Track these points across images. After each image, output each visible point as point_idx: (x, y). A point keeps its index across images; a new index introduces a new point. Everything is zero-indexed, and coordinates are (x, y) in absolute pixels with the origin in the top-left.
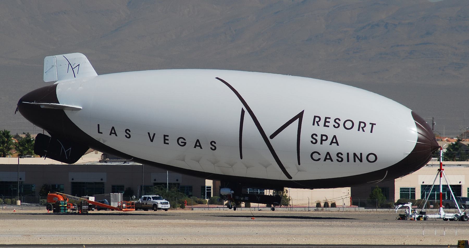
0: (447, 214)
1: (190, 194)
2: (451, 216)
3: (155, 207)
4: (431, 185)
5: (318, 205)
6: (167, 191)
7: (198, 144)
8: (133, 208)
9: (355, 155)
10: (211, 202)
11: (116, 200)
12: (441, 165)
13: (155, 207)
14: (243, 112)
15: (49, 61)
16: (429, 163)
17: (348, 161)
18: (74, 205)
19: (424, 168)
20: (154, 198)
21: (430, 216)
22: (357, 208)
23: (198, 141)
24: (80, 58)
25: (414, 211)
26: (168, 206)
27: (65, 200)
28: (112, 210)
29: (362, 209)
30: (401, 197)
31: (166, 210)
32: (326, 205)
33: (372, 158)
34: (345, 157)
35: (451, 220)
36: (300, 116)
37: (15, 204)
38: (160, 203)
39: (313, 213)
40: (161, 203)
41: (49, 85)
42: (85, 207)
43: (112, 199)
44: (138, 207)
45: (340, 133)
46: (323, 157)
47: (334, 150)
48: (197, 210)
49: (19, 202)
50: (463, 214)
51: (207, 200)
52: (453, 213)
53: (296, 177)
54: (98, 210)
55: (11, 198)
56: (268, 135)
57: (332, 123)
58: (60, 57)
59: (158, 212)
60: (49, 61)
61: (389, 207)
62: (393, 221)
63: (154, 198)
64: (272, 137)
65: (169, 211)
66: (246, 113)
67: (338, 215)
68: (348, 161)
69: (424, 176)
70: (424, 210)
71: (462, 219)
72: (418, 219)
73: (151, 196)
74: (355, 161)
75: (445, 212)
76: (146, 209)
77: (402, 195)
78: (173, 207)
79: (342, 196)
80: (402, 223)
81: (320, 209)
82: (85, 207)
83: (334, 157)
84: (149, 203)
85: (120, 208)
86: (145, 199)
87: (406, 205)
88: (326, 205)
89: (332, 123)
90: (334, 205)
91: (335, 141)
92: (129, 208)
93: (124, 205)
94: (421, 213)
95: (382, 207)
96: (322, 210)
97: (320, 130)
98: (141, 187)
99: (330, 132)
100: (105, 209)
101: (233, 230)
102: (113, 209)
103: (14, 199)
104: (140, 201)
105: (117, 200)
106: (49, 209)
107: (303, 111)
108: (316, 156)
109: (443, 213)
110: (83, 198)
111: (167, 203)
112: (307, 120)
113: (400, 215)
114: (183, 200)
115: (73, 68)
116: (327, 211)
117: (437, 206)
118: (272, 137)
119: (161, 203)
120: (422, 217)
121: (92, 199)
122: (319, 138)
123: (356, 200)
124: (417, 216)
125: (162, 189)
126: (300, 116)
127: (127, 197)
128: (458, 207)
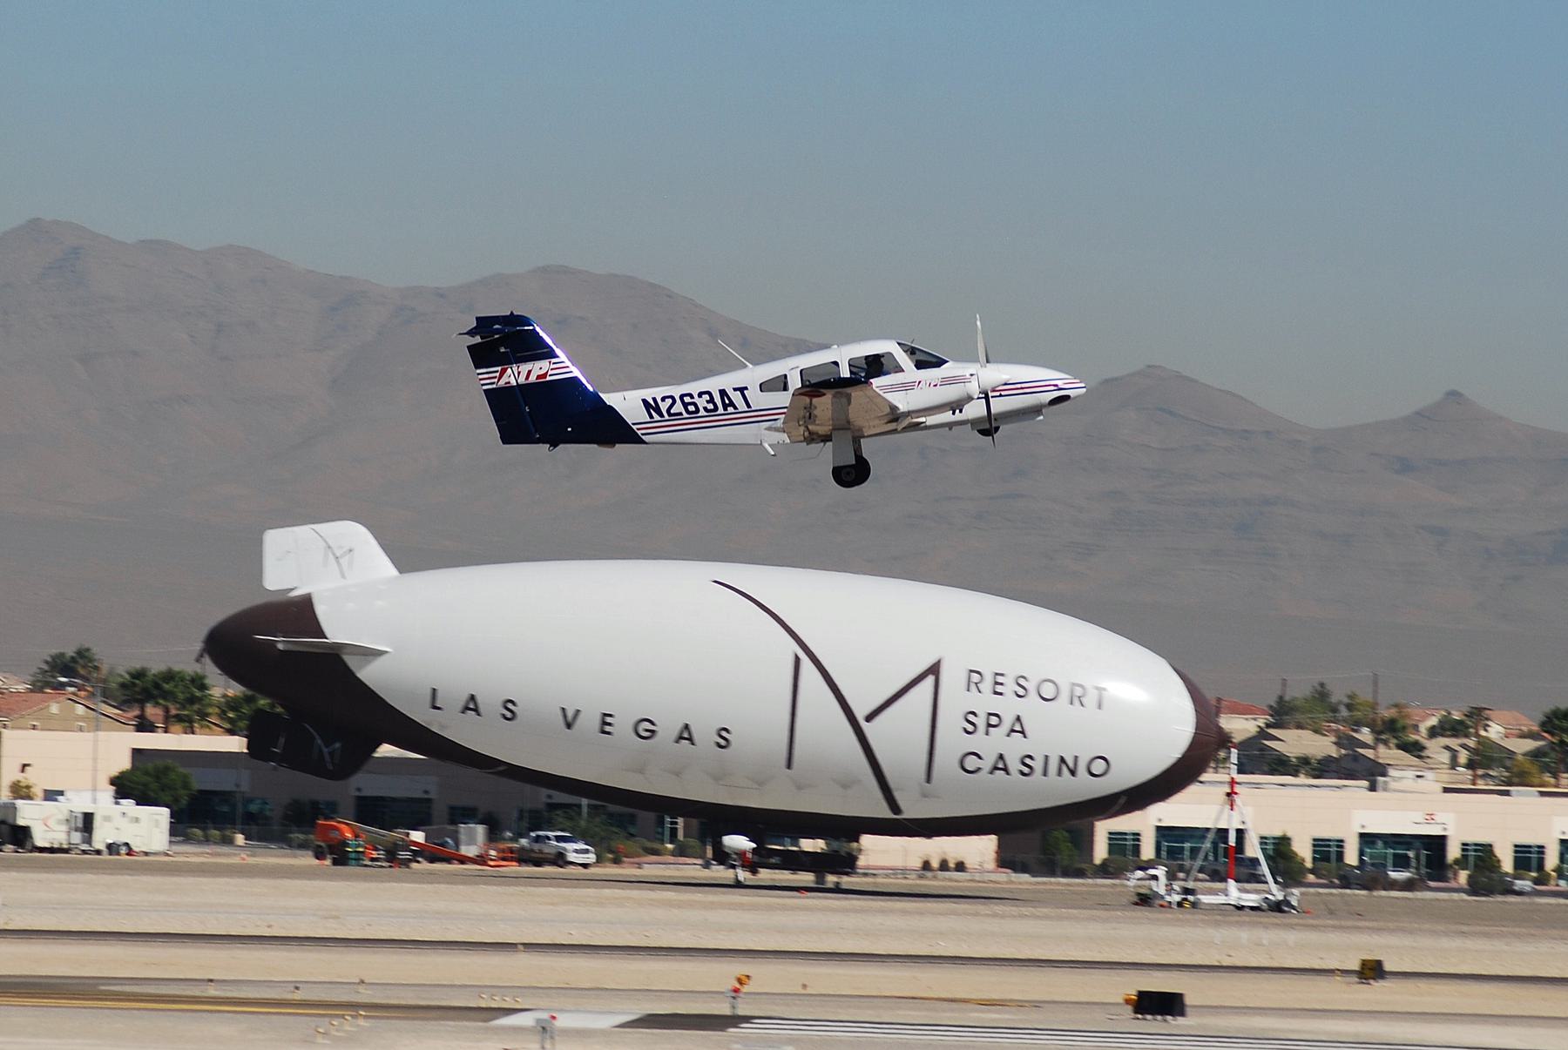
0: (1245, 896)
1: (632, 830)
2: (1251, 899)
3: (560, 860)
4: (1208, 829)
5: (926, 866)
6: (583, 823)
7: (686, 735)
8: (512, 860)
9: (1062, 760)
10: (681, 852)
11: (472, 842)
12: (1233, 783)
13: (560, 860)
14: (797, 660)
15: (277, 541)
16: (1204, 777)
17: (1045, 774)
18: (376, 849)
19: (1193, 789)
20: (558, 839)
21: (1206, 899)
22: (1015, 877)
23: (687, 727)
24: (354, 535)
25: (1170, 890)
26: (591, 858)
27: (356, 836)
28: (462, 862)
29: (1026, 877)
30: (1110, 852)
31: (585, 866)
32: (944, 866)
33: (1099, 767)
34: (1037, 765)
35: (1252, 908)
36: (934, 670)
37: (228, 841)
38: (575, 851)
39: (912, 883)
40: (576, 851)
41: (280, 598)
42: (404, 855)
43: (463, 837)
44: (524, 858)
45: (1030, 708)
46: (987, 764)
47: (1014, 749)
48: (652, 869)
49: (240, 839)
50: (1280, 897)
51: (670, 846)
52: (1257, 892)
53: (911, 811)
54: (432, 861)
55: (204, 829)
56: (860, 716)
57: (1009, 687)
58: (304, 532)
59: (570, 870)
60: (277, 541)
61: (1080, 874)
62: (1123, 907)
63: (558, 839)
64: (869, 718)
65: (592, 870)
66: (806, 661)
67: (968, 888)
68: (1045, 774)
69: (1192, 808)
70: (1190, 885)
71: (1278, 907)
72: (1180, 904)
73: (550, 834)
74: (1060, 773)
75: (1240, 890)
76: (538, 864)
77: (1112, 848)
78: (600, 860)
79: (980, 850)
80: (1143, 912)
81: (929, 874)
82: (404, 855)
83: (1014, 765)
84: (546, 850)
85: (481, 860)
86: (538, 839)
87: (1152, 872)
88: (944, 866)
89: (1009, 687)
90: (960, 867)
91: (1019, 728)
92: (504, 859)
93: (493, 853)
94: (1187, 891)
95: (1065, 874)
96: (935, 877)
97: (984, 703)
98: (521, 811)
99: (1008, 707)
100: (448, 860)
101: (780, 919)
102: (463, 860)
103: (228, 833)
104: (524, 842)
105: (473, 839)
106: (319, 855)
107: (939, 662)
108: (971, 763)
109: (1234, 893)
110: (397, 834)
111: (587, 851)
112: (952, 678)
113: (1139, 894)
114: (613, 844)
115: (338, 556)
116: (945, 879)
117: (1218, 876)
118: (869, 718)
119: (576, 851)
120: (1188, 901)
121: (418, 836)
122: (980, 722)
123: (1005, 860)
124: (1177, 898)
125: (571, 819)
126: (934, 670)
127: (493, 836)
128: (1269, 878)
